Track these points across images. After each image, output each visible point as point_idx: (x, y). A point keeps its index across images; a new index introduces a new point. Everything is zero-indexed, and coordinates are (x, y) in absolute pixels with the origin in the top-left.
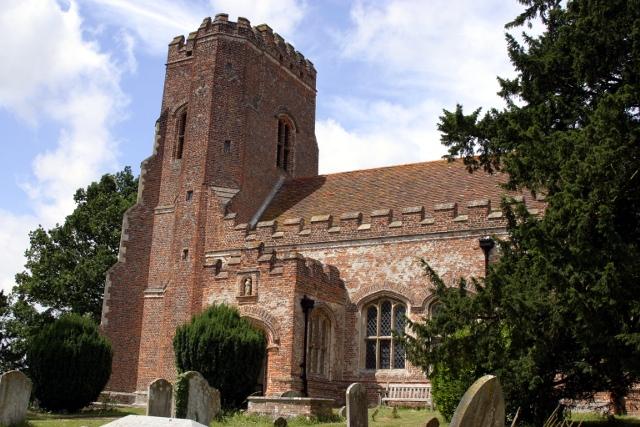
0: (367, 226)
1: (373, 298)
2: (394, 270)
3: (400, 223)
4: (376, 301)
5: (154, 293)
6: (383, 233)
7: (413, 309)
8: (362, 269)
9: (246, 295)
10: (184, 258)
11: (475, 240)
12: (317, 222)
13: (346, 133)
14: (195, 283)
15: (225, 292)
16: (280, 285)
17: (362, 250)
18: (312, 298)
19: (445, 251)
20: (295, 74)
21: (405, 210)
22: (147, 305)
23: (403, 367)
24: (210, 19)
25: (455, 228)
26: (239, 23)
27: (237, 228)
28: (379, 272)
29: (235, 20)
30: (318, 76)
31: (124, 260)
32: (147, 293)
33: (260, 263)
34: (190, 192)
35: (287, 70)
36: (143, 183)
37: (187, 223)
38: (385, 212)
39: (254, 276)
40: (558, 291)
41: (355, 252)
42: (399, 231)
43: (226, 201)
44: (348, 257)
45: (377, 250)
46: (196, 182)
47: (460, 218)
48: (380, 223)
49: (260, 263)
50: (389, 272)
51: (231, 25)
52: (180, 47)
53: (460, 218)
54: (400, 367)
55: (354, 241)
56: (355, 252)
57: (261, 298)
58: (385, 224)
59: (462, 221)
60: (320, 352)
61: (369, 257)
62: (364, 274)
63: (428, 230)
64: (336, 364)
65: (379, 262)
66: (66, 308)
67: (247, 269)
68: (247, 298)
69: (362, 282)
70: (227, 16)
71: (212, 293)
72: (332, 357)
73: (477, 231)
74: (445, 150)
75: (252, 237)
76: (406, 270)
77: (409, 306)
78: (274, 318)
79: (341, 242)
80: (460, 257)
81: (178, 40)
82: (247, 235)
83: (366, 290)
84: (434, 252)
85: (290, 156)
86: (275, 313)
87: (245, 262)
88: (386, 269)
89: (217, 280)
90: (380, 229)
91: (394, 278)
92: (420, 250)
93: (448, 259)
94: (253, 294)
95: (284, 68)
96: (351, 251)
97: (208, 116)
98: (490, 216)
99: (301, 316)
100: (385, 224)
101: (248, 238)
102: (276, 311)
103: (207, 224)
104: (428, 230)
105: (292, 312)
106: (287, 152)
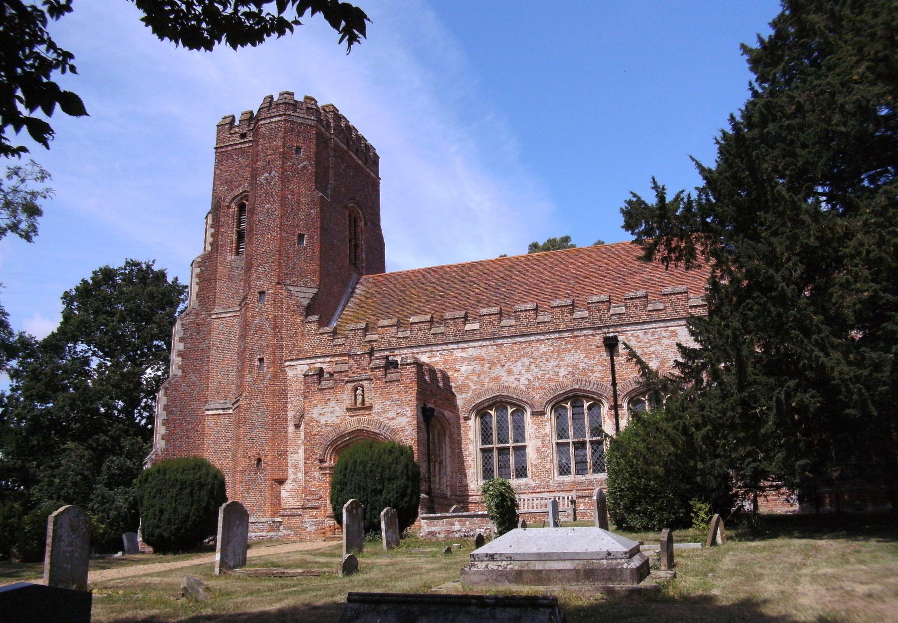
0: (476, 326)
1: (486, 404)
2: (510, 372)
3: (513, 322)
5: (217, 409)
9: (359, 406)
10: (259, 367)
11: (597, 338)
12: (416, 323)
13: (142, 258)
15: (332, 403)
17: (470, 352)
18: (430, 405)
19: (565, 350)
20: (360, 159)
21: (412, 320)
22: (210, 423)
23: (526, 476)
24: (272, 97)
25: (574, 325)
26: (305, 102)
27: (320, 332)
28: (493, 375)
29: (772, 32)
30: (381, 163)
31: (180, 373)
32: (208, 410)
33: (372, 369)
34: (262, 293)
35: (354, 156)
36: (197, 284)
37: (260, 328)
38: (495, 310)
39: (365, 383)
41: (464, 355)
43: (306, 302)
44: (456, 360)
45: (487, 350)
46: (269, 281)
47: (577, 314)
49: (372, 369)
51: (295, 105)
52: (231, 128)
53: (577, 314)
54: (521, 477)
55: (464, 339)
56: (464, 355)
57: (377, 408)
59: (582, 318)
60: (437, 464)
61: (480, 359)
62: (475, 378)
63: (541, 328)
64: (452, 478)
65: (492, 364)
67: (356, 376)
68: (359, 409)
69: (473, 387)
70: (292, 94)
72: (449, 469)
73: (600, 328)
76: (523, 371)
77: (529, 411)
78: (393, 430)
79: (447, 344)
80: (582, 356)
81: (228, 121)
83: (479, 395)
85: (359, 252)
86: (393, 424)
87: (354, 369)
88: (499, 371)
91: (509, 381)
92: (538, 349)
93: (569, 358)
95: (351, 153)
96: (459, 354)
99: (423, 426)
101: (336, 342)
103: (284, 328)
104: (341, 350)
105: (415, 422)
106: (356, 246)
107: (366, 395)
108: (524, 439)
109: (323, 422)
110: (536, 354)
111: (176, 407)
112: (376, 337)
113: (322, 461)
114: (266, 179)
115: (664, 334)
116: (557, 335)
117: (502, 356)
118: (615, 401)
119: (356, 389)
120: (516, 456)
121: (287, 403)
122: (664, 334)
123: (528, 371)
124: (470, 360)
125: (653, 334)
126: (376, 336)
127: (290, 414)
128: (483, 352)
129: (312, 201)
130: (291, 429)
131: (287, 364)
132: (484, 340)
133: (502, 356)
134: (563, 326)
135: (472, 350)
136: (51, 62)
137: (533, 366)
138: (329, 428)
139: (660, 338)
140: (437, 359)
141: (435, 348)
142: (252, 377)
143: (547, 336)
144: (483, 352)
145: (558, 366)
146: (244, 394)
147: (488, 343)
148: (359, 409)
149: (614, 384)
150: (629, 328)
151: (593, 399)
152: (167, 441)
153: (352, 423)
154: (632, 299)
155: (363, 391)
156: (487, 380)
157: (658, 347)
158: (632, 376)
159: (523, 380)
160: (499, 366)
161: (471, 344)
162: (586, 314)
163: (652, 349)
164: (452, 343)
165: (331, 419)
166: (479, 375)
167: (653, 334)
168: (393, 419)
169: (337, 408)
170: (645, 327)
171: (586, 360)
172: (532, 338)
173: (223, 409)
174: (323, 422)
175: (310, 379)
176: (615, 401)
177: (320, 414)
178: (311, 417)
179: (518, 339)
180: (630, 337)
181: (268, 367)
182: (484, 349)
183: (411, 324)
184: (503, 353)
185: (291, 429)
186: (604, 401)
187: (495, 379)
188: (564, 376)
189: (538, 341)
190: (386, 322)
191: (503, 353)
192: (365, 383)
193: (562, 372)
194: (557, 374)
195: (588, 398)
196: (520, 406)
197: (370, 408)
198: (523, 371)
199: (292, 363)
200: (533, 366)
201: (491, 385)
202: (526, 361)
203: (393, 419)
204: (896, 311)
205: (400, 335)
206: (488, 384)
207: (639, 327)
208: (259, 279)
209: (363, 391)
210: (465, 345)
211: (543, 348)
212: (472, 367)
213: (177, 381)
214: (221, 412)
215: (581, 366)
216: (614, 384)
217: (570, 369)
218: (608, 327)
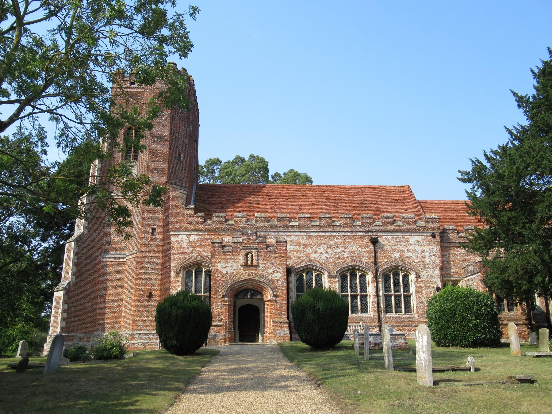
1: (301, 269)
2: (316, 252)
3: (318, 223)
4: (303, 271)
6: (308, 228)
7: (330, 277)
8: (293, 250)
10: (153, 233)
12: (259, 217)
14: (163, 253)
16: (275, 258)
17: (292, 238)
19: (348, 243)
21: (256, 215)
23: (514, 311)
28: (305, 253)
39: (254, 252)
42: (318, 227)
45: (303, 239)
51: (179, 72)
53: (356, 224)
57: (261, 266)
58: (308, 223)
61: (298, 243)
62: (295, 254)
63: (398, 229)
65: (305, 247)
68: (249, 266)
69: (294, 259)
71: (220, 262)
73: (368, 232)
75: (208, 223)
76: (324, 252)
79: (278, 232)
80: (358, 247)
82: (205, 221)
84: (341, 243)
86: (272, 277)
88: (309, 251)
89: (223, 252)
90: (305, 226)
91: (315, 256)
93: (350, 247)
94: (255, 263)
97: (168, 133)
98: (374, 224)
100: (308, 223)
101: (206, 223)
102: (273, 276)
104: (209, 228)
108: (366, 291)
109: (225, 272)
111: (83, 254)
115: (402, 239)
116: (343, 234)
117: (311, 242)
119: (247, 254)
120: (361, 300)
121: (170, 258)
122: (402, 239)
123: (326, 252)
125: (397, 239)
127: (173, 265)
129: (186, 134)
133: (311, 242)
134: (347, 229)
138: (228, 276)
139: (400, 241)
140: (272, 240)
142: (147, 239)
143: (338, 234)
145: (344, 251)
148: (249, 266)
149: (376, 264)
150: (384, 234)
151: (363, 271)
152: (76, 276)
153: (245, 275)
154: (386, 218)
156: (302, 255)
157: (399, 246)
158: (385, 260)
159: (323, 257)
160: (309, 248)
161: (293, 233)
162: (360, 223)
163: (396, 247)
164: (281, 231)
165: (230, 271)
166: (297, 252)
167: (397, 239)
169: (234, 265)
170: (392, 234)
171: (360, 249)
172: (329, 234)
173: (115, 258)
175: (216, 245)
177: (223, 268)
178: (217, 269)
179: (321, 234)
180: (383, 239)
181: (159, 234)
182: (301, 237)
183: (256, 217)
184: (312, 240)
185: (173, 274)
186: (369, 273)
189: (332, 236)
190: (240, 215)
191: (312, 240)
193: (346, 255)
194: (343, 255)
195: (403, 271)
197: (257, 266)
198: (324, 252)
199: (175, 233)
201: (305, 258)
202: (326, 246)
204: (551, 238)
207: (389, 234)
209: (252, 255)
210: (290, 234)
211: (335, 240)
213: (85, 237)
214: (113, 260)
215: (357, 252)
218: (372, 232)
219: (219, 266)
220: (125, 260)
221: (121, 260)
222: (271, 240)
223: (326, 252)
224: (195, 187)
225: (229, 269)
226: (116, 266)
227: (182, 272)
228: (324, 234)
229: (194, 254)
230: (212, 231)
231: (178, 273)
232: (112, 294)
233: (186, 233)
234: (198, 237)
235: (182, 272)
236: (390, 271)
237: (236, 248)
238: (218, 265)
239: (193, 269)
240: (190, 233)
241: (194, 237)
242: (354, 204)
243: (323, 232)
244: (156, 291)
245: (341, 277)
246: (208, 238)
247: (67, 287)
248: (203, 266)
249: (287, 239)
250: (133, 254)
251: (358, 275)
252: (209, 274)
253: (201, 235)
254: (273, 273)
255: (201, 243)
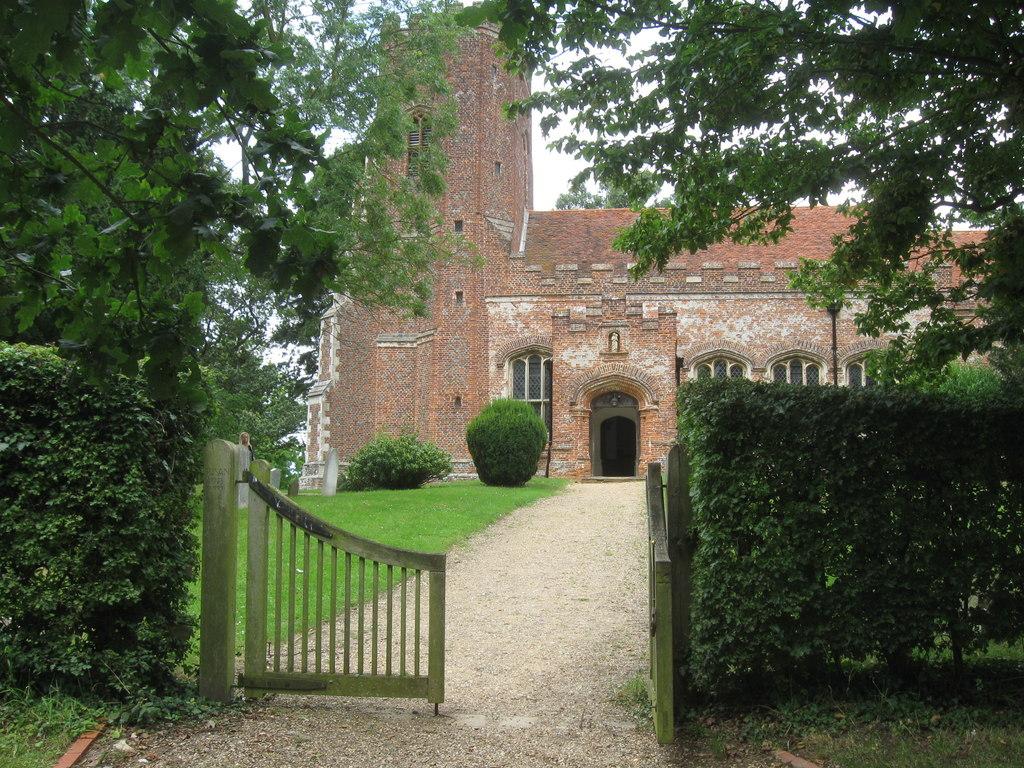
2: (731, 328)
4: (709, 361)
5: (391, 342)
8: (693, 325)
15: (585, 347)
17: (691, 305)
32: (380, 342)
39: (621, 329)
40: (533, 312)
41: (685, 307)
42: (736, 287)
45: (710, 306)
48: (713, 277)
49: (629, 317)
50: (724, 328)
55: (685, 290)
57: (634, 355)
61: (701, 313)
62: (695, 331)
63: (765, 287)
65: (714, 319)
66: (989, 683)
68: (614, 354)
71: (566, 348)
74: (921, 118)
76: (745, 329)
79: (667, 294)
91: (731, 337)
92: (760, 308)
93: (792, 319)
96: (679, 305)
107: (622, 341)
109: (574, 365)
110: (759, 312)
112: (589, 280)
113: (572, 404)
114: (461, 97)
116: (781, 296)
118: (835, 364)
121: (487, 342)
124: (691, 312)
126: (590, 280)
127: (492, 353)
128: (705, 306)
130: (492, 368)
131: (487, 300)
132: (706, 293)
135: (694, 303)
136: (627, 34)
137: (755, 324)
141: (653, 297)
144: (705, 306)
145: (781, 326)
146: (439, 329)
147: (710, 297)
149: (834, 348)
151: (812, 360)
153: (607, 369)
155: (619, 337)
156: (708, 334)
159: (745, 337)
160: (720, 321)
161: (693, 297)
166: (699, 329)
168: (651, 367)
169: (589, 352)
171: (808, 323)
172: (756, 296)
173: (399, 342)
174: (574, 365)
176: (835, 364)
179: (741, 296)
184: (725, 308)
185: (492, 368)
187: (716, 334)
188: (786, 337)
190: (601, 267)
191: (725, 308)
192: (621, 329)
193: (785, 333)
194: (779, 334)
196: (740, 362)
200: (755, 324)
202: (749, 319)
203: (651, 367)
205: (616, 280)
206: (709, 337)
208: (455, 206)
209: (619, 337)
210: (686, 297)
211: (766, 307)
212: (692, 320)
215: (803, 328)
216: (834, 348)
217: (792, 331)
219: (565, 355)
220: (415, 345)
221: (409, 345)
222: (649, 310)
223: (750, 327)
224: (526, 216)
225: (580, 359)
226: (402, 356)
227: (506, 364)
228: (746, 297)
229: (527, 335)
230: (555, 296)
231: (500, 366)
232: (397, 401)
233: (513, 299)
234: (532, 306)
235: (506, 364)
236: (861, 360)
237: (591, 325)
238: (564, 354)
239: (532, 361)
240: (519, 299)
241: (526, 307)
242: (805, 240)
243: (744, 293)
244: (466, 395)
245: (775, 370)
246: (548, 307)
247: (328, 390)
248: (542, 354)
249: (679, 305)
250: (428, 336)
251: (805, 366)
252: (549, 365)
253: (537, 302)
254: (651, 366)
255: (538, 316)
